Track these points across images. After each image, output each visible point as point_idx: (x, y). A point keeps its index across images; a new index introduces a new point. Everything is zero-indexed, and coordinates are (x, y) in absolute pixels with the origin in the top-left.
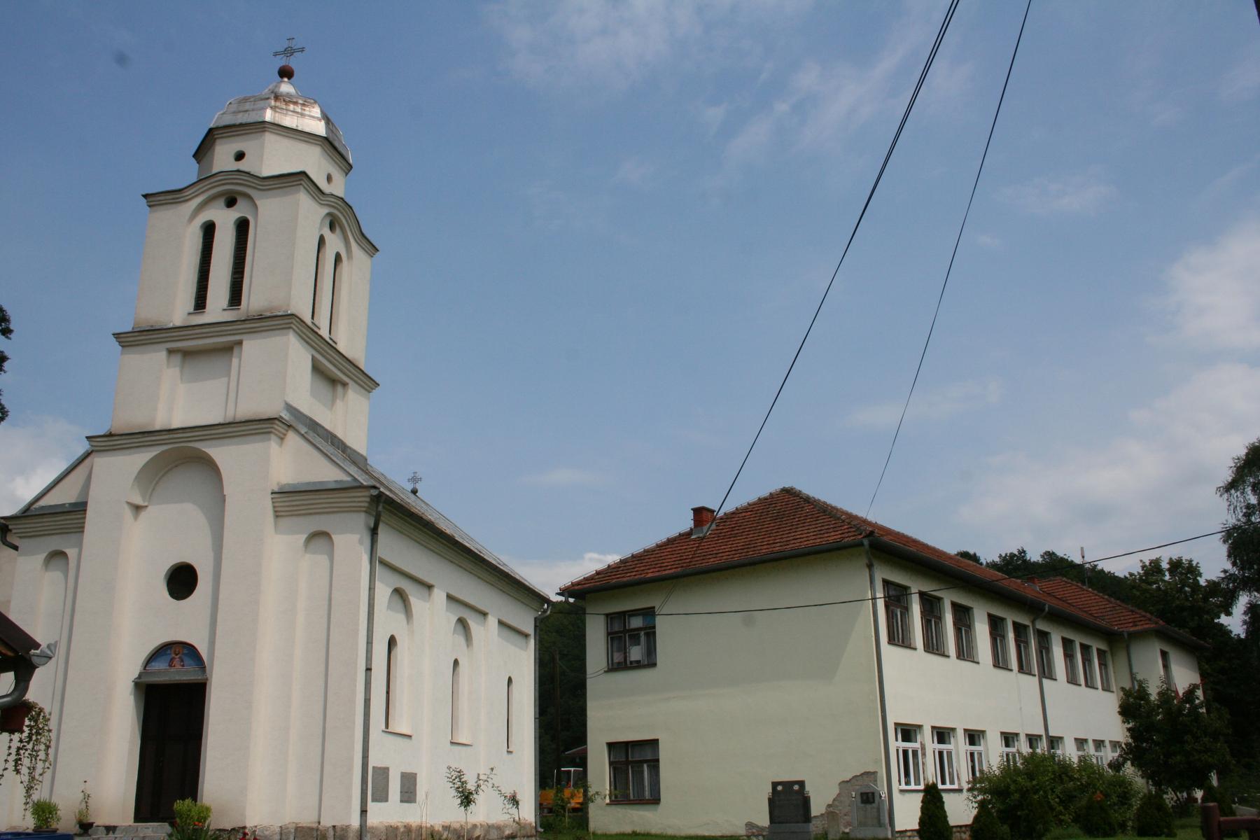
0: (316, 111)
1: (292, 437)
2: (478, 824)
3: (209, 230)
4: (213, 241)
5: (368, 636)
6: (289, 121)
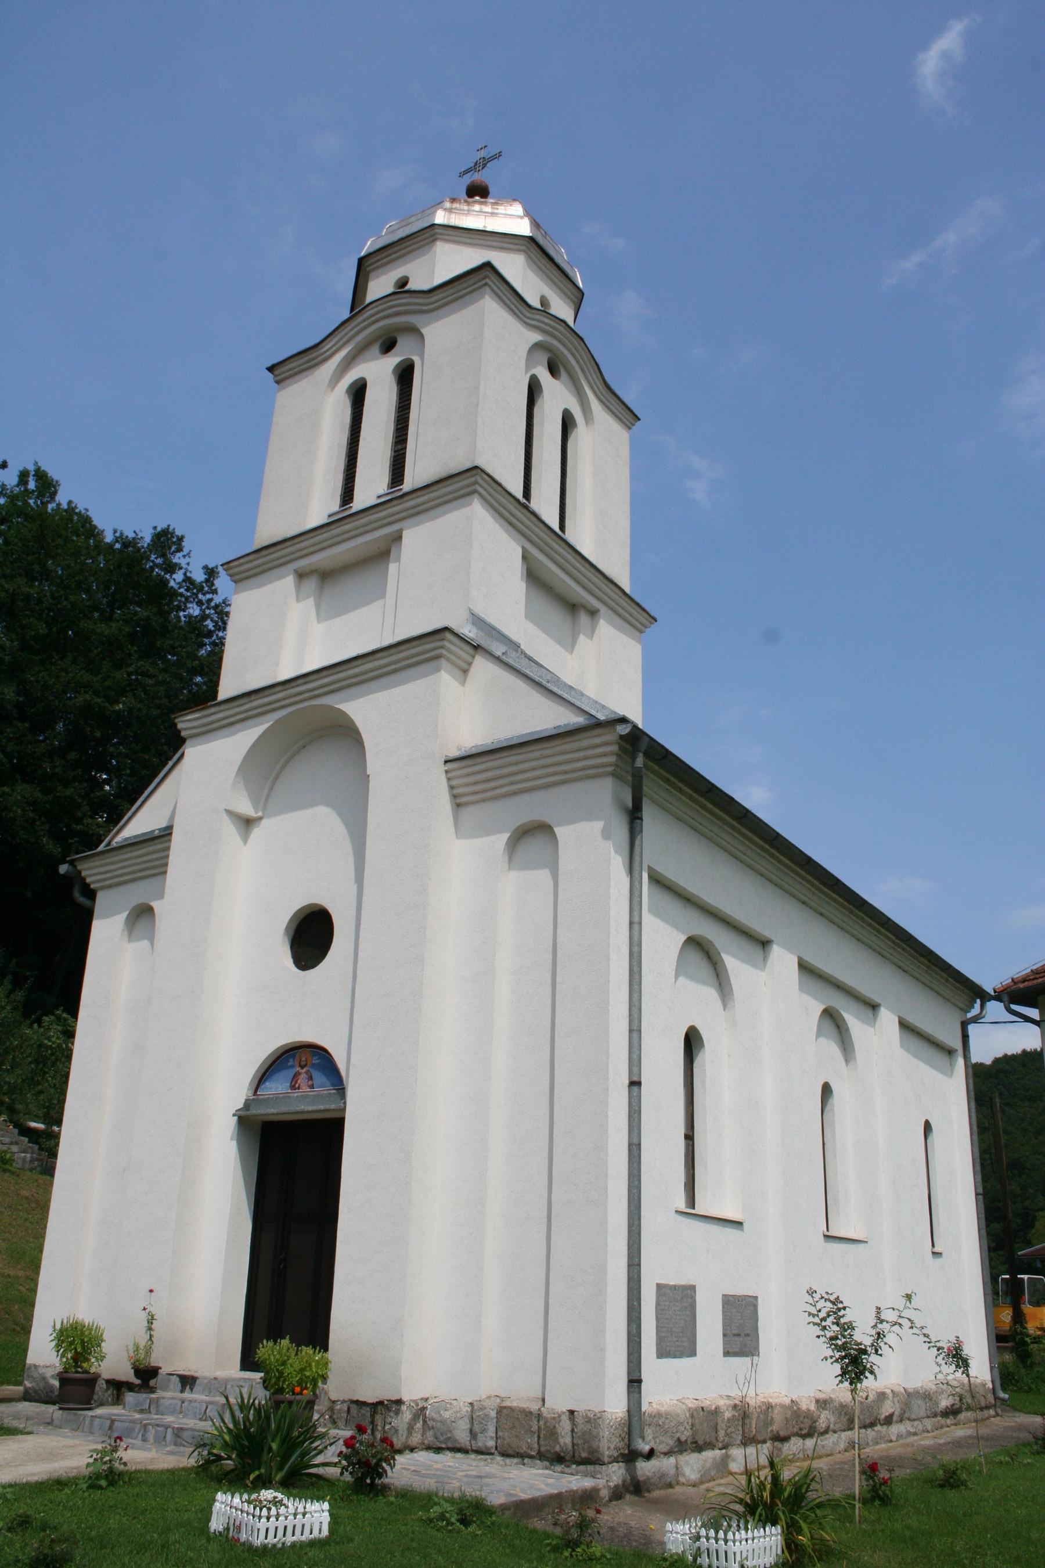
1: (481, 665)
2: (888, 1391)
3: (358, 393)
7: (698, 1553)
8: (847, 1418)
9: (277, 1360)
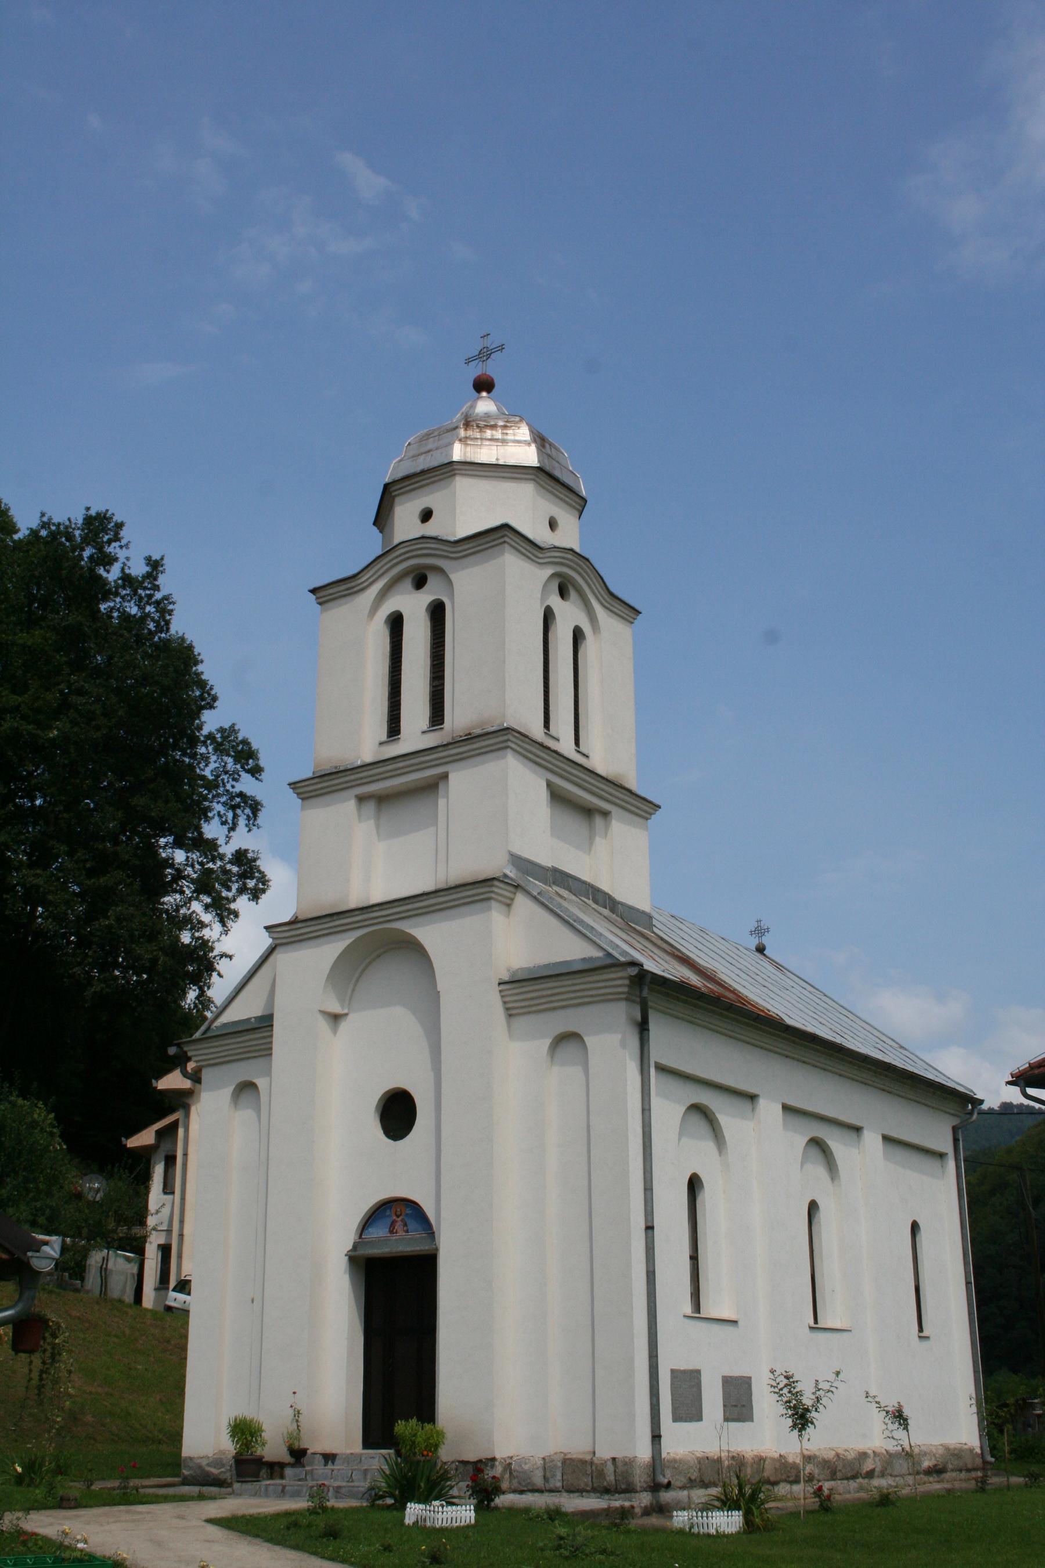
0: (523, 432)
2: (870, 1452)
3: (396, 623)
4: (402, 640)
5: (645, 1178)
6: (486, 454)
7: (692, 1527)
8: (830, 1470)
9: (410, 1434)
